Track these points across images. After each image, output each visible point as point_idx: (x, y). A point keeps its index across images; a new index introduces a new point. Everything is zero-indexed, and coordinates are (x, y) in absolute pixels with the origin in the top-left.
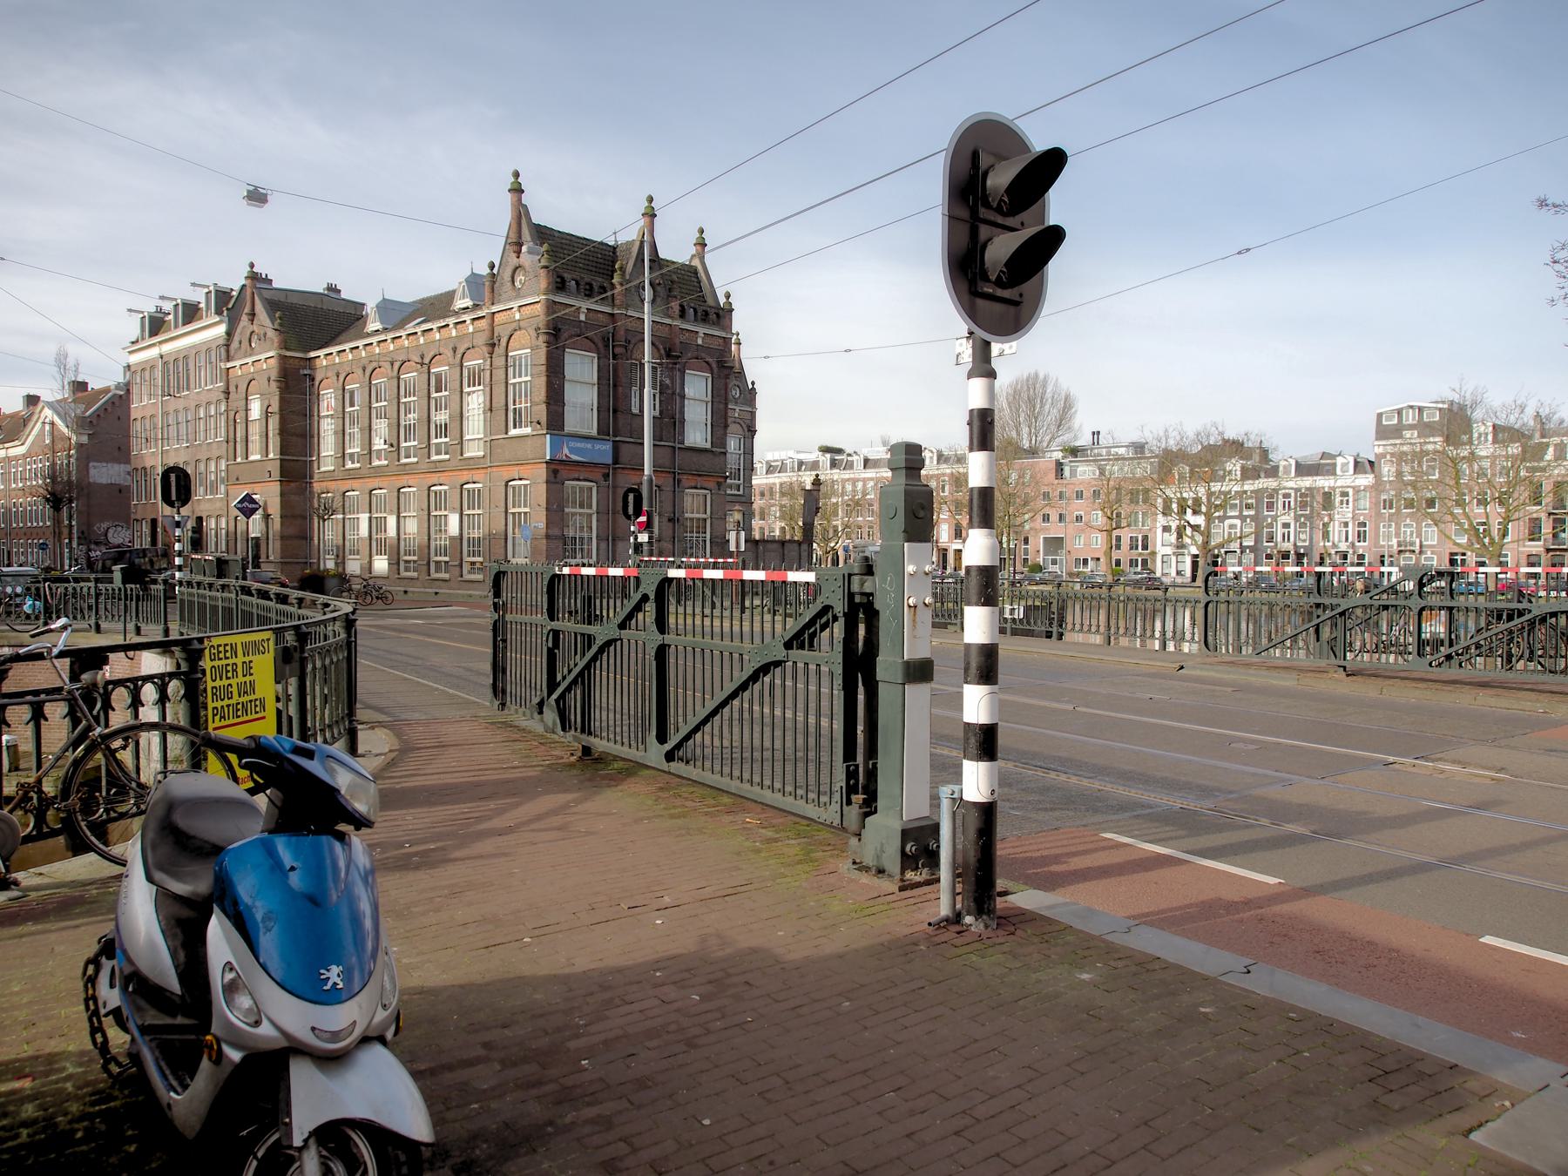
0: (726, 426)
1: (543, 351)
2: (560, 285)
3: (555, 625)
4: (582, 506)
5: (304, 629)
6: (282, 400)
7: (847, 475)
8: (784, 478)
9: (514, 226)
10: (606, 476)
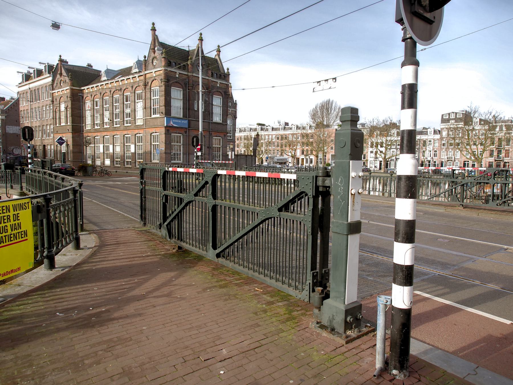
0: (227, 115)
1: (163, 88)
2: (169, 64)
3: (166, 192)
4: (177, 142)
5: (49, 197)
6: (72, 104)
7: (266, 133)
8: (245, 134)
9: (153, 43)
10: (186, 132)
